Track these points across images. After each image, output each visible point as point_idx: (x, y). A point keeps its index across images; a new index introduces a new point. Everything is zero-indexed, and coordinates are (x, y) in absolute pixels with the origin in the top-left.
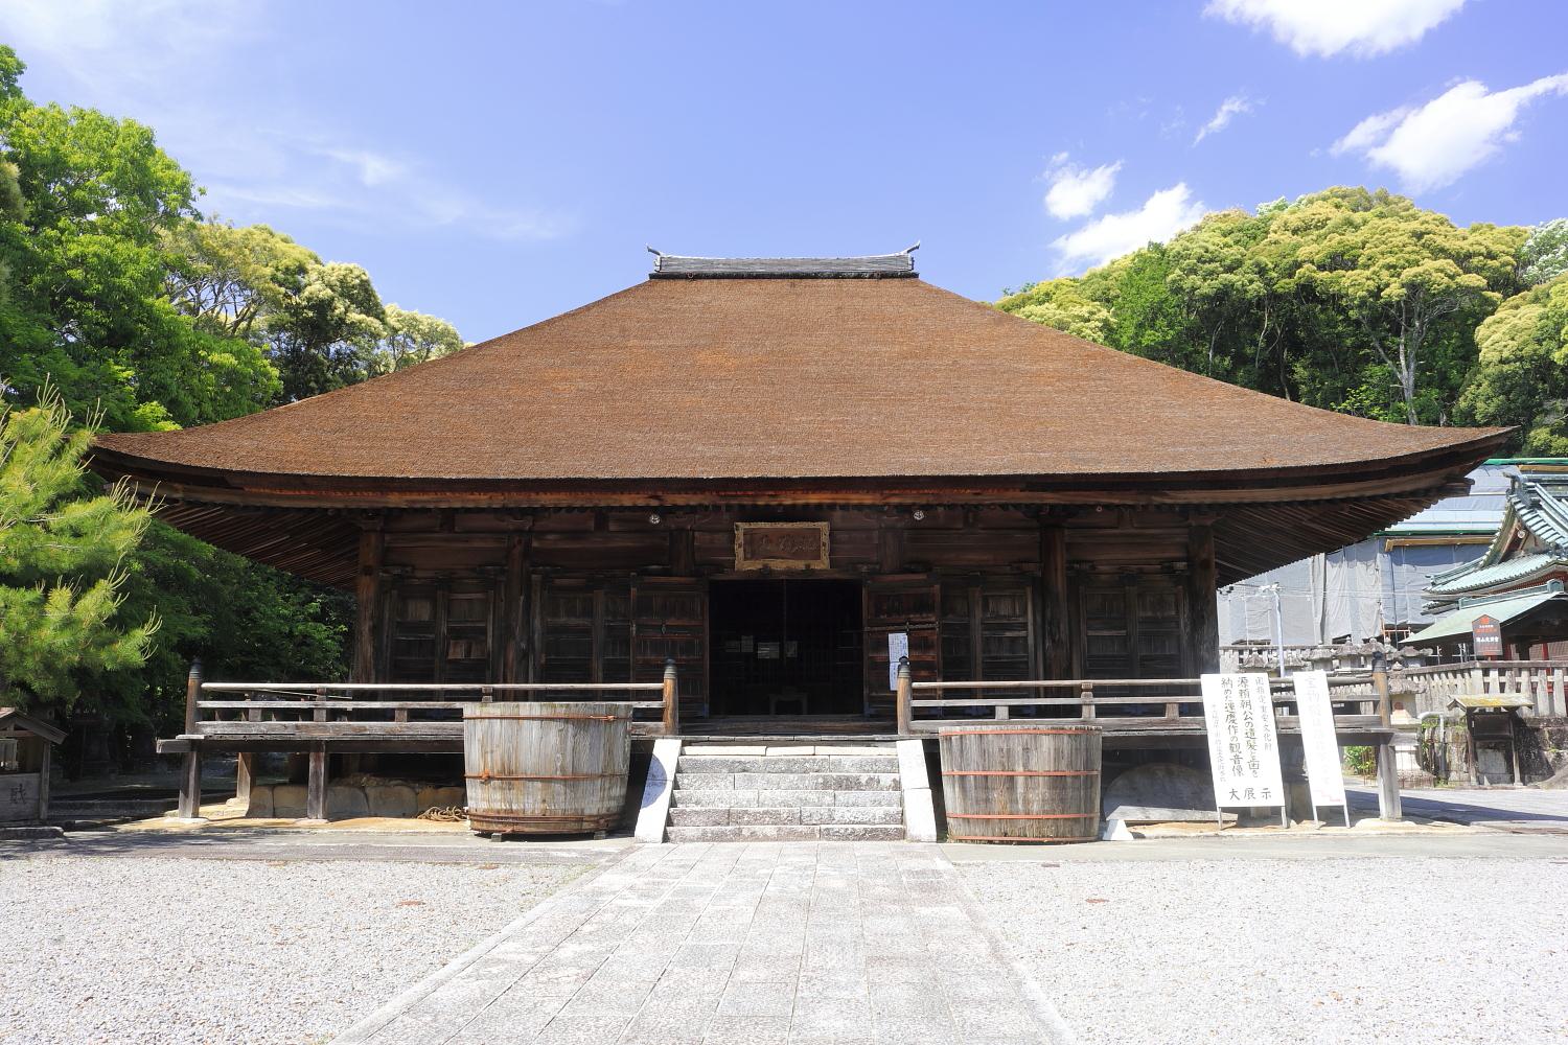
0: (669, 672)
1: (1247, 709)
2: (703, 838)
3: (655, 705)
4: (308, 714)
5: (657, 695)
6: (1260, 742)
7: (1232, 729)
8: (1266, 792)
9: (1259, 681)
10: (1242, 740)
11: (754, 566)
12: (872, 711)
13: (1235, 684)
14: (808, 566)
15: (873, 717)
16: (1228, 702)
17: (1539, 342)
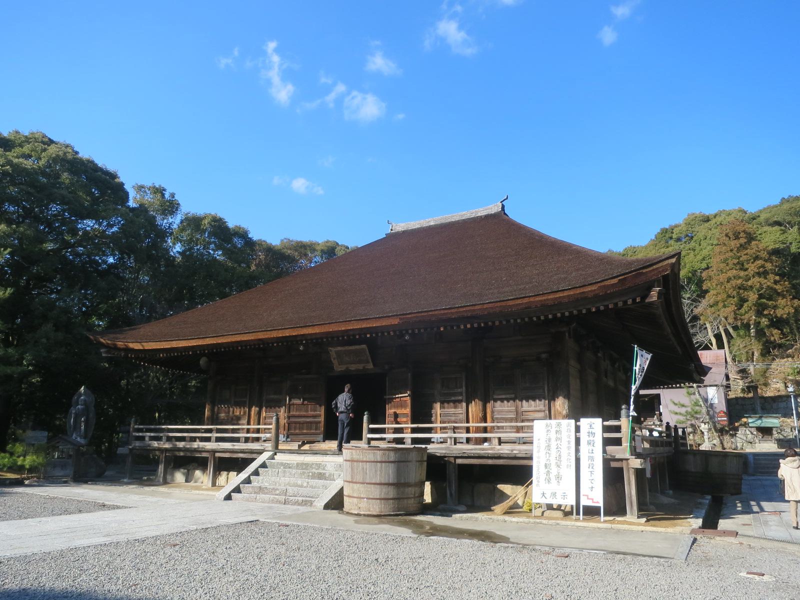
1: (559, 442)
6: (564, 463)
7: (548, 455)
8: (564, 496)
9: (569, 425)
10: (553, 462)
13: (554, 426)
14: (364, 367)
16: (548, 437)
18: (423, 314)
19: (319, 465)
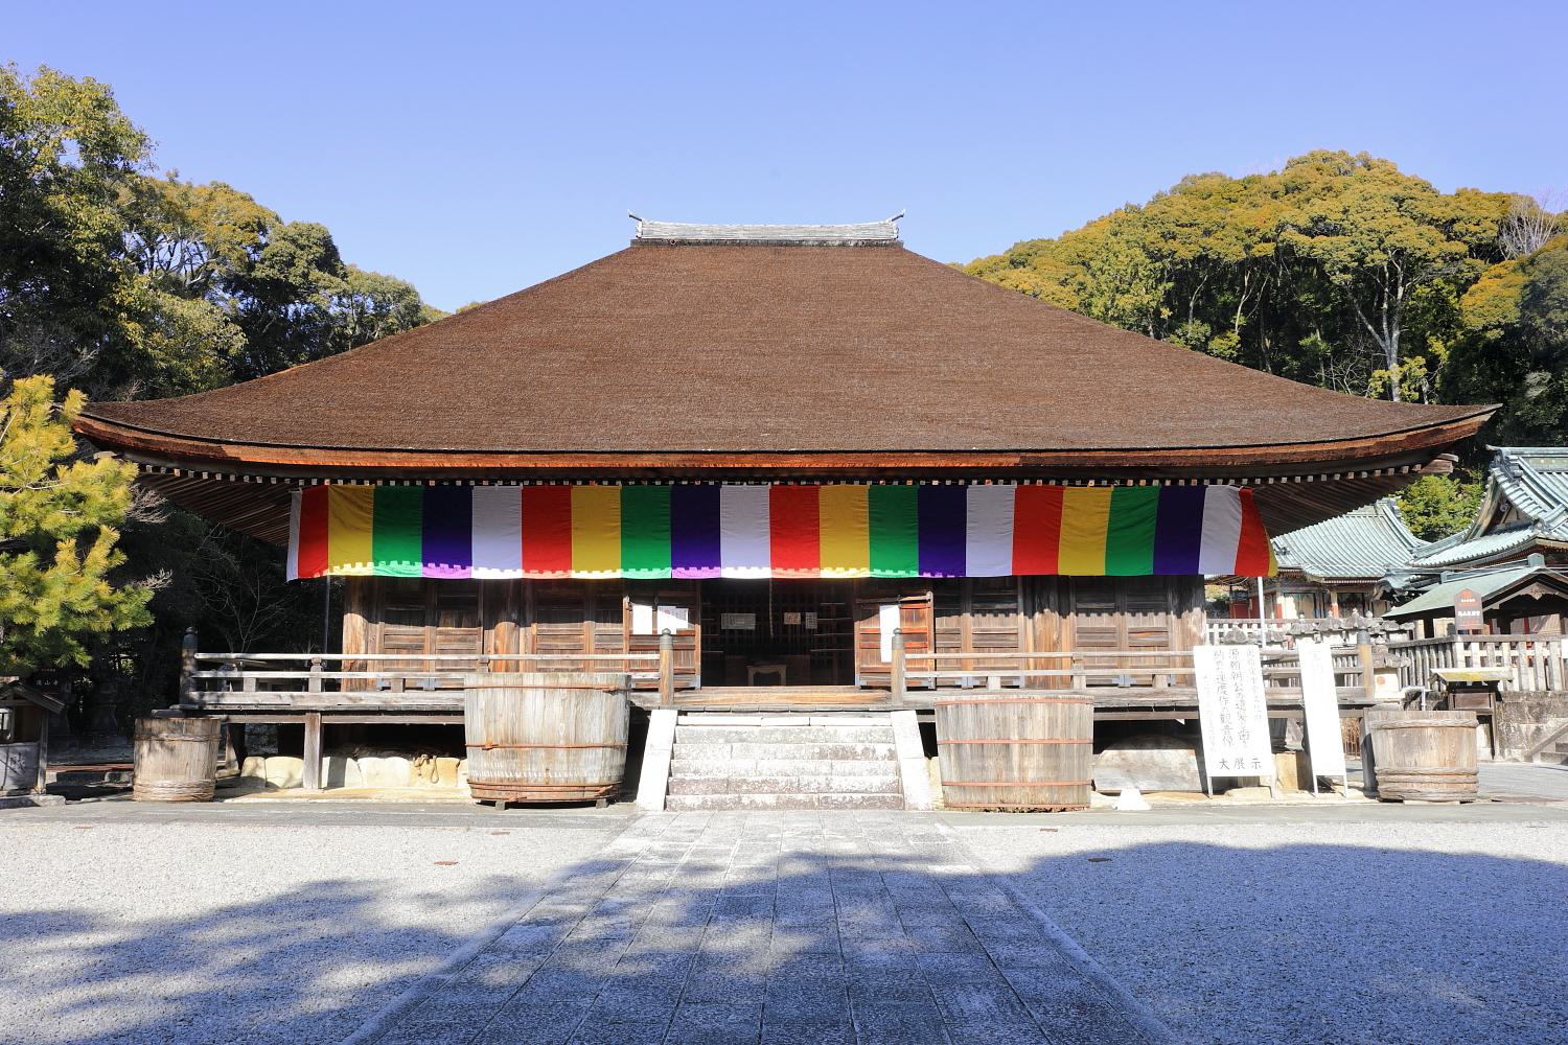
1: (1238, 681)
4: (301, 685)
5: (654, 666)
8: (1256, 763)
12: (864, 684)
15: (863, 687)
18: (1071, 454)
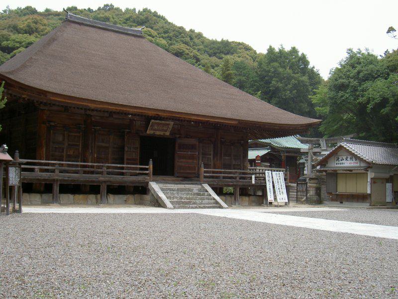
0: (151, 162)
2: (367, 208)
3: (147, 172)
5: (147, 169)
11: (152, 132)
12: (178, 175)
15: (178, 177)
17: (353, 67)
19: (189, 190)
